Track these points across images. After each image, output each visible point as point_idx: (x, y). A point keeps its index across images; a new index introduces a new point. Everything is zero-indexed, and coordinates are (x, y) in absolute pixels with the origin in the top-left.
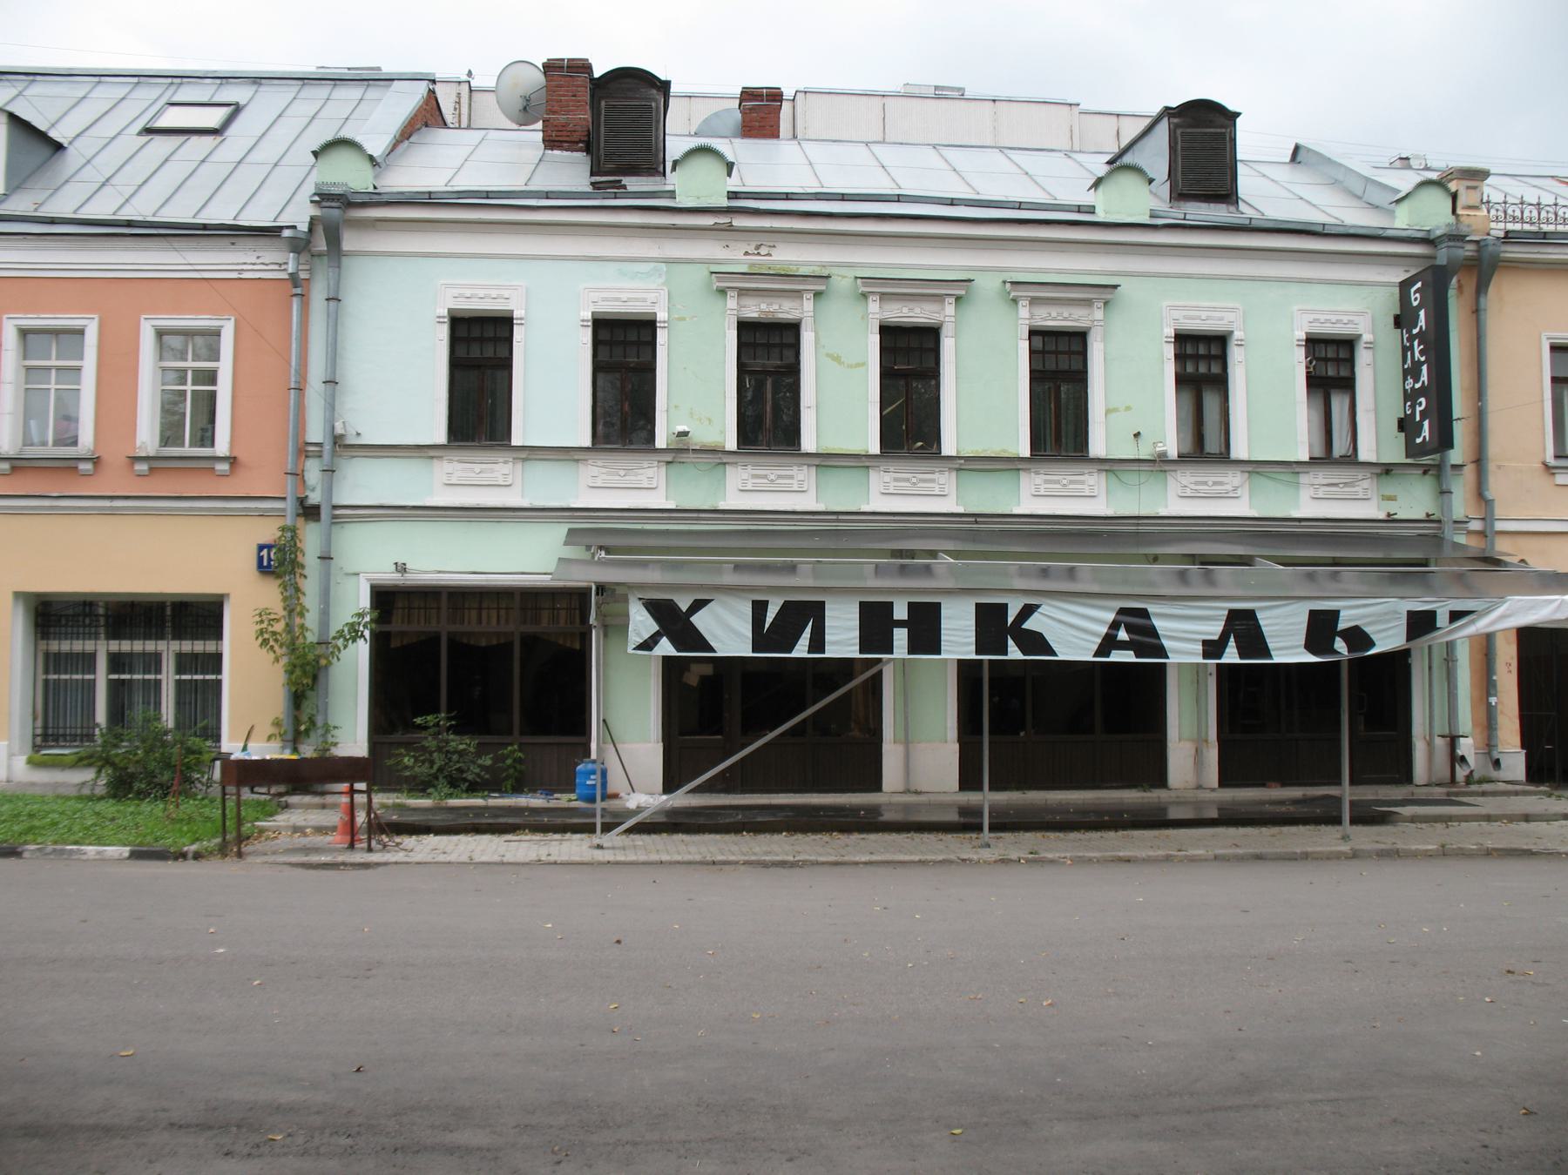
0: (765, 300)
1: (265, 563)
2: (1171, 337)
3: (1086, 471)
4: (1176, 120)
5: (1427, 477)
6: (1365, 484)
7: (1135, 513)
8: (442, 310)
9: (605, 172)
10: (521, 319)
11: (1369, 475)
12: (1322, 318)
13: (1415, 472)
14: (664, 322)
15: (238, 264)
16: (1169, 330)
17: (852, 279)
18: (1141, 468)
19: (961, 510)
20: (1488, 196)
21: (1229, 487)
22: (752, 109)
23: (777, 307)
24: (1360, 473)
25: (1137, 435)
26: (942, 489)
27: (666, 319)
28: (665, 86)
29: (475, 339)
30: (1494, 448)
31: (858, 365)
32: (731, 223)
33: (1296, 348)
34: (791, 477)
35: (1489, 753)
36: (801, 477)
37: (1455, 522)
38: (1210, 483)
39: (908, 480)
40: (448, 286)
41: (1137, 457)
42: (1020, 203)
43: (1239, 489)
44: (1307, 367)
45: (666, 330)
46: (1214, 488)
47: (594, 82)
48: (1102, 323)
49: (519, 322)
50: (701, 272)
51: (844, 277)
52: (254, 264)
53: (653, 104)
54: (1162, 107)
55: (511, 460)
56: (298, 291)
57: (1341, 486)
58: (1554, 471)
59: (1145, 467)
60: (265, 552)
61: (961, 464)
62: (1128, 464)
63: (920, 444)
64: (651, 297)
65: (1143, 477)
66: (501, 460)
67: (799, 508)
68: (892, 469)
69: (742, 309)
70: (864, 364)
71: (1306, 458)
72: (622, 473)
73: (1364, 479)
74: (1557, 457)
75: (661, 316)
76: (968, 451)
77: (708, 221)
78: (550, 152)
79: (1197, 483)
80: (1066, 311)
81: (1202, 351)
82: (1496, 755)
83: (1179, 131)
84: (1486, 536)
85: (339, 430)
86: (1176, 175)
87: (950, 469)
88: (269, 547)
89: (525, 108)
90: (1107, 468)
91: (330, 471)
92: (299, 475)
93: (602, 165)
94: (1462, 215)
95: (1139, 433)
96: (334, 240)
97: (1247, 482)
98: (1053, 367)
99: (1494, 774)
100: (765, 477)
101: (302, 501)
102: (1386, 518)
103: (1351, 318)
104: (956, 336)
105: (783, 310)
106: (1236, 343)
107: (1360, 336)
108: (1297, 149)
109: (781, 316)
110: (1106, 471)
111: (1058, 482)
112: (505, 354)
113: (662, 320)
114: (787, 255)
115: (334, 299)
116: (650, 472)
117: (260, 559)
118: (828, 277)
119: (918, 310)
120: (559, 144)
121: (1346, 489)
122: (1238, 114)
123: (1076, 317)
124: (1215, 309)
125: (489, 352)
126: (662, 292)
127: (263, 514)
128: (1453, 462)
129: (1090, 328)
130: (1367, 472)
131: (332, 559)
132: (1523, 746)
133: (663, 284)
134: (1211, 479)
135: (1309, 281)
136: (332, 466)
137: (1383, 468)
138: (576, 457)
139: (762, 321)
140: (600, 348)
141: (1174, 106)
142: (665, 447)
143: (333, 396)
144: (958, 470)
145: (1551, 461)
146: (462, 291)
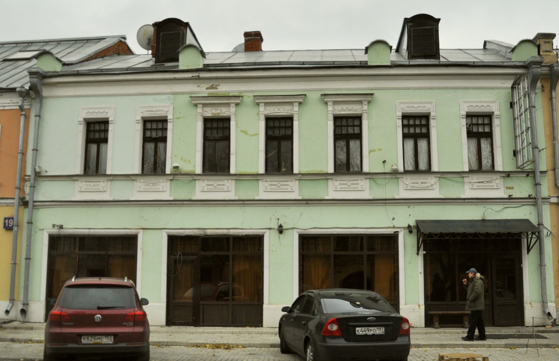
0: (215, 108)
2: (400, 116)
3: (359, 179)
4: (410, 24)
5: (528, 177)
6: (498, 181)
7: (384, 197)
10: (112, 121)
11: (499, 177)
12: (474, 105)
13: (523, 175)
15: (3, 104)
16: (399, 113)
18: (386, 177)
21: (429, 185)
25: (384, 162)
26: (362, 187)
29: (154, 129)
31: (254, 135)
32: (199, 75)
34: (224, 185)
36: (228, 185)
37: (543, 199)
38: (420, 183)
39: (276, 185)
40: (84, 109)
41: (384, 172)
42: (334, 62)
43: (434, 185)
45: (172, 123)
46: (422, 185)
48: (367, 111)
49: (111, 122)
50: (186, 98)
51: (249, 97)
52: (9, 103)
53: (181, 32)
55: (106, 180)
57: (485, 182)
59: (387, 176)
60: (7, 221)
61: (300, 177)
62: (245, 176)
64: (166, 109)
65: (387, 181)
66: (102, 181)
67: (227, 198)
68: (269, 180)
69: (205, 113)
70: (258, 134)
71: (466, 169)
72: (151, 185)
73: (496, 179)
75: (170, 117)
76: (304, 171)
77: (189, 75)
79: (413, 183)
80: (350, 107)
81: (418, 122)
83: (412, 29)
85: (38, 170)
88: (9, 219)
91: (33, 187)
92: (21, 189)
94: (543, 55)
97: (438, 182)
98: (340, 133)
100: (212, 185)
102: (508, 197)
104: (299, 120)
105: (222, 112)
106: (496, 117)
107: (493, 113)
109: (221, 115)
110: (370, 178)
111: (346, 184)
112: (290, 133)
114: (224, 88)
115: (39, 116)
116: (163, 185)
117: (5, 224)
119: (282, 109)
121: (487, 184)
122: (438, 20)
123: (355, 109)
124: (421, 103)
125: (283, 132)
126: (170, 107)
127: (7, 205)
130: (498, 176)
134: (420, 181)
135: (457, 88)
138: (133, 179)
139: (214, 118)
143: (36, 156)
144: (299, 180)
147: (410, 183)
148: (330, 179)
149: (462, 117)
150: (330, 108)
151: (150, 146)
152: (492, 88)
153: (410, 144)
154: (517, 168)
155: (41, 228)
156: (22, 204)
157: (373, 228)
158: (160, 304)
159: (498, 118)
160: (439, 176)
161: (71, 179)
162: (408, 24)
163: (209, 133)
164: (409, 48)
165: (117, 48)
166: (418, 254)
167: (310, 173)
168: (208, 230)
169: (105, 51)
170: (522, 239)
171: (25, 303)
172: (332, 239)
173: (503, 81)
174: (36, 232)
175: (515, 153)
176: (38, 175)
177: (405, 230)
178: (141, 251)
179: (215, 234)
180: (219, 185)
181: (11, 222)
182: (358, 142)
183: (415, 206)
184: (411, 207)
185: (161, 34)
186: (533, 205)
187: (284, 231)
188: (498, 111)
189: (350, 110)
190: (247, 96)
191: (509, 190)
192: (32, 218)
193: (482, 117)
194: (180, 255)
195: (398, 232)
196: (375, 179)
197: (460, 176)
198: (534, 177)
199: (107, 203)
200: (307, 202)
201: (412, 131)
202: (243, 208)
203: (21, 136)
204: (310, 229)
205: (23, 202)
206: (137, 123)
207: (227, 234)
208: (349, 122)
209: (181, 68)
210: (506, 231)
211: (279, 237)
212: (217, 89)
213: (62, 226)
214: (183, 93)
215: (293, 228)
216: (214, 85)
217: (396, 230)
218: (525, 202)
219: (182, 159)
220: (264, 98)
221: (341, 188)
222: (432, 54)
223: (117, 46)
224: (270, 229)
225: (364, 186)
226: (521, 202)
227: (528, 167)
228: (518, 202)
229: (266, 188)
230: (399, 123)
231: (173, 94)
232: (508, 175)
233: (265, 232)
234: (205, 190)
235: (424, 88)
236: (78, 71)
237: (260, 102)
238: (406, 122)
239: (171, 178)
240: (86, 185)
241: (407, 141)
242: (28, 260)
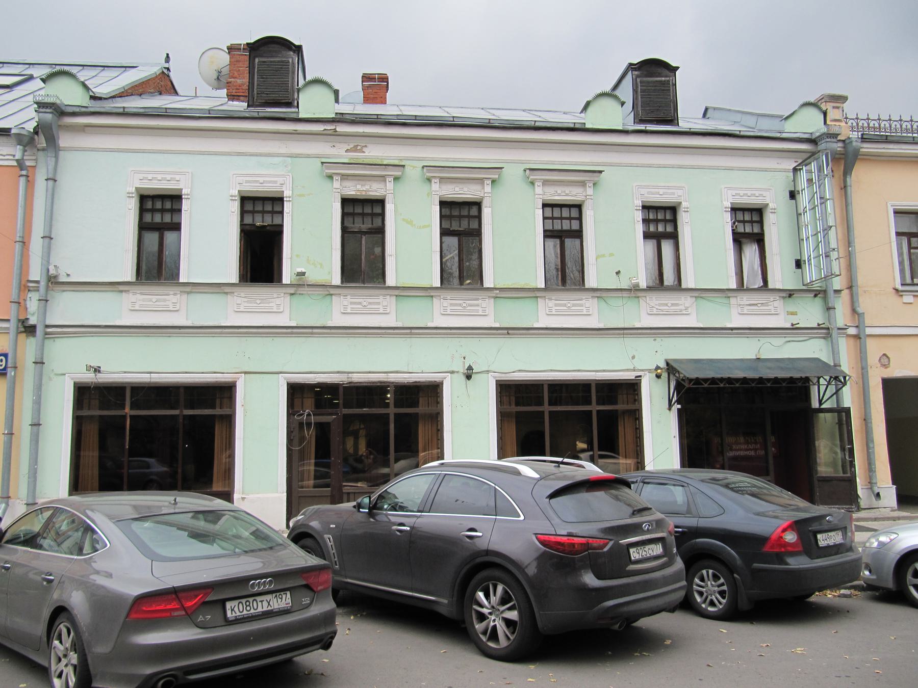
0: (360, 182)
2: (639, 206)
4: (636, 73)
6: (776, 303)
8: (131, 189)
9: (257, 105)
10: (188, 195)
11: (778, 298)
12: (742, 193)
14: (289, 197)
16: (234, 191)
17: (420, 169)
18: (624, 295)
19: (497, 325)
20: (846, 114)
21: (682, 307)
22: (369, 86)
24: (771, 297)
25: (618, 273)
26: (484, 311)
27: (290, 195)
28: (298, 49)
30: (861, 279)
31: (424, 227)
34: (378, 304)
35: (871, 488)
37: (839, 329)
38: (669, 305)
43: (689, 309)
44: (732, 227)
45: (291, 203)
47: (250, 46)
51: (414, 167)
54: (627, 63)
55: (179, 292)
56: (24, 173)
58: (901, 294)
59: (625, 294)
61: (497, 294)
63: (468, 281)
64: (280, 180)
66: (172, 293)
72: (258, 301)
73: (774, 301)
74: (902, 285)
75: (287, 193)
77: (319, 128)
78: (231, 102)
79: (660, 305)
80: (567, 190)
82: (876, 490)
83: (638, 80)
84: (860, 338)
85: (52, 271)
86: (637, 108)
87: (489, 297)
89: (218, 78)
90: (598, 295)
92: (20, 304)
93: (255, 100)
94: (831, 125)
95: (619, 272)
96: (52, 141)
99: (875, 503)
100: (360, 303)
101: (23, 322)
103: (761, 193)
105: (373, 190)
108: (706, 109)
110: (598, 297)
111: (565, 305)
113: (288, 195)
114: (374, 152)
116: (278, 301)
118: (403, 166)
119: (466, 189)
120: (237, 97)
122: (677, 68)
124: (669, 188)
125: (167, 218)
128: (835, 288)
129: (584, 201)
130: (776, 296)
132: (893, 484)
136: (46, 297)
137: (788, 293)
138: (226, 291)
140: (246, 215)
141: (636, 63)
142: (289, 283)
145: (900, 288)
146: (145, 175)
147: (656, 305)
148: (125, 291)
149: (725, 210)
150: (539, 190)
151: (152, 238)
152: (766, 170)
153: (553, 243)
154: (803, 285)
155: (60, 372)
156: (23, 329)
157: (604, 371)
158: (277, 495)
161: (115, 289)
162: (634, 73)
163: (348, 224)
164: (635, 106)
165: (158, 83)
166: (670, 409)
169: (144, 86)
170: (811, 387)
171: (31, 501)
172: (182, 390)
173: (780, 161)
174: (50, 379)
175: (798, 264)
176: (53, 280)
177: (650, 374)
178: (243, 408)
179: (366, 380)
182: (578, 241)
183: (481, 339)
184: (658, 339)
185: (257, 60)
186: (824, 338)
187: (473, 376)
188: (773, 203)
189: (567, 195)
190: (411, 166)
191: (791, 316)
192: (42, 354)
193: (646, 209)
195: (640, 376)
196: (605, 299)
197: (724, 296)
198: (825, 299)
199: (182, 330)
200: (508, 331)
201: (558, 226)
202: (408, 339)
203: (20, 211)
204: (513, 372)
205: (25, 327)
206: (232, 200)
207: (386, 380)
208: (659, 214)
209: (301, 116)
210: (755, 375)
211: (466, 384)
212: (364, 152)
213: (100, 367)
214: (308, 156)
215: (488, 372)
216: (358, 145)
220: (439, 170)
222: (668, 119)
223: (159, 79)
224: (452, 372)
225: (591, 309)
227: (816, 286)
229: (445, 310)
230: (639, 216)
232: (790, 294)
235: (673, 167)
236: (124, 108)
237: (386, 175)
238: (446, 211)
239: (292, 291)
240: (144, 300)
241: (653, 244)
242: (35, 428)
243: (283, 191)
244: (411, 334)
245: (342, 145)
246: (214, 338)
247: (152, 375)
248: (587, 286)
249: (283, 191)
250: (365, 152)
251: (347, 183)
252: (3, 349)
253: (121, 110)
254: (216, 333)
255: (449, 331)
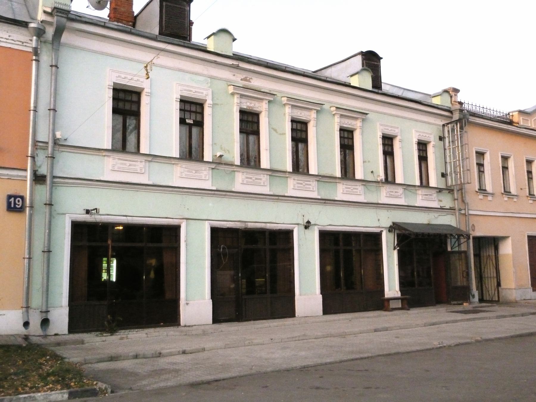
0: (249, 101)
1: (12, 206)
11: (208, 169)
19: (319, 197)
23: (253, 105)
25: (372, 172)
29: (187, 111)
32: (238, 65)
33: (107, 89)
34: (261, 179)
45: (149, 97)
55: (144, 161)
60: (12, 200)
61: (320, 179)
64: (205, 92)
73: (205, 170)
74: (479, 189)
85: (58, 135)
88: (15, 197)
100: (251, 178)
106: (146, 94)
109: (255, 109)
110: (364, 185)
114: (257, 82)
117: (9, 204)
122: (382, 58)
131: (53, 205)
133: (209, 87)
135: (397, 116)
148: (108, 156)
159: (148, 95)
160: (405, 187)
163: (255, 128)
167: (326, 175)
168: (249, 223)
180: (256, 179)
181: (19, 201)
183: (392, 211)
184: (389, 211)
194: (224, 248)
204: (327, 226)
217: (382, 229)
218: (449, 212)
219: (221, 148)
221: (298, 187)
224: (298, 224)
226: (447, 212)
228: (445, 212)
231: (212, 78)
232: (440, 190)
233: (295, 228)
234: (245, 183)
240: (122, 164)
243: (206, 100)
244: (278, 199)
245: (239, 75)
246: (115, 190)
247: (128, 217)
248: (204, 160)
249: (206, 100)
250: (251, 82)
251: (244, 100)
252: (16, 193)
253: (103, 24)
254: (197, 193)
255: (297, 199)
